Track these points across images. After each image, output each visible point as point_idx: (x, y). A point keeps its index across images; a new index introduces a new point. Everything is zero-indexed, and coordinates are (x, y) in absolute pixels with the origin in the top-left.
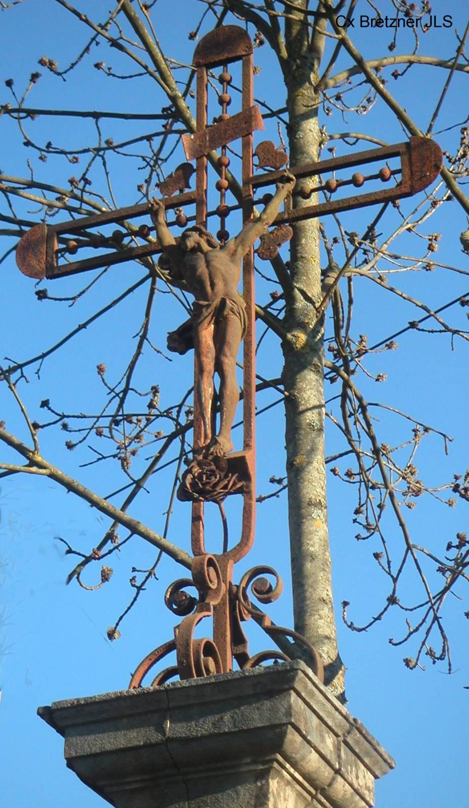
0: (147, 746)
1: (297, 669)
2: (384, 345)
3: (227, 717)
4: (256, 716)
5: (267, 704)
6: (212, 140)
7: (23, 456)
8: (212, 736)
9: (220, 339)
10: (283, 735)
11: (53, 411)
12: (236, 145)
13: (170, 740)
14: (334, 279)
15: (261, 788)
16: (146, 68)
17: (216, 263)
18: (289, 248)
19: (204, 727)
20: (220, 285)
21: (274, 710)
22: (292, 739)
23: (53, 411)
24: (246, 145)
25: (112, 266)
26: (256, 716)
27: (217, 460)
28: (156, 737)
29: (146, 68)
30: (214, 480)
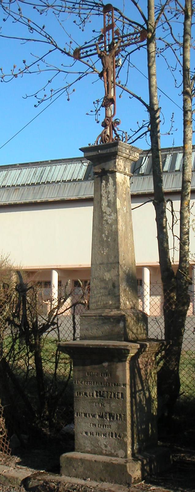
0: (96, 155)
1: (116, 172)
2: (34, 96)
3: (108, 150)
4: (113, 150)
5: (114, 148)
6: (107, 30)
7: (184, 19)
8: (106, 153)
9: (107, 75)
10: (117, 153)
11: (173, 37)
12: (111, 31)
13: (99, 154)
14: (128, 53)
15: (80, 459)
16: (90, 9)
17: (106, 60)
18: (157, 236)
19: (104, 152)
20: (107, 64)
21: (115, 149)
22: (119, 153)
23: (173, 37)
24: (113, 31)
25: (182, 77)
26: (113, 150)
27: (108, 99)
28: (98, 153)
29: (90, 9)
30: (108, 103)
